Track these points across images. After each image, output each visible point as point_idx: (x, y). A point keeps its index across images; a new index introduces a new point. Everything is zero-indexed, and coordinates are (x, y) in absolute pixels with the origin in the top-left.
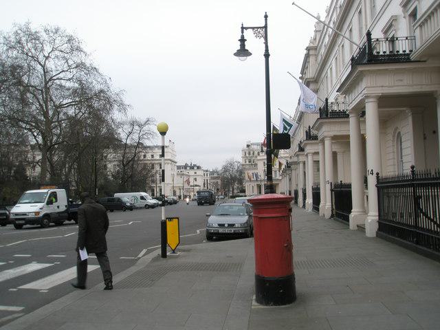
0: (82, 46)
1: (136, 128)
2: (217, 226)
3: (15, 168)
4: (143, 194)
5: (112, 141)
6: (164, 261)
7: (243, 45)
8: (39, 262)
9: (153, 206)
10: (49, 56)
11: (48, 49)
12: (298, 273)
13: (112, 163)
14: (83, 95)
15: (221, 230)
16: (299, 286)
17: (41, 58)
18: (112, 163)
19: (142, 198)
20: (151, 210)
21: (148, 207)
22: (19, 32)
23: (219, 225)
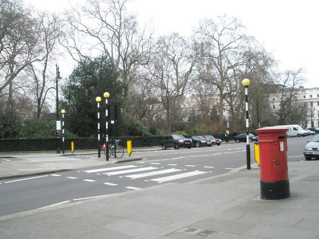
0: (243, 23)
1: (291, 76)
2: (311, 149)
3: (211, 111)
4: (295, 126)
5: (274, 88)
6: (250, 172)
7: (59, 75)
8: (200, 170)
9: (304, 135)
10: (221, 34)
11: (220, 29)
12: (291, 181)
13: (275, 103)
14: (250, 56)
15: (314, 153)
16: (292, 189)
17: (216, 36)
18: (275, 103)
19: (295, 129)
20: (302, 138)
21: (299, 135)
22: (201, 21)
23: (313, 149)
